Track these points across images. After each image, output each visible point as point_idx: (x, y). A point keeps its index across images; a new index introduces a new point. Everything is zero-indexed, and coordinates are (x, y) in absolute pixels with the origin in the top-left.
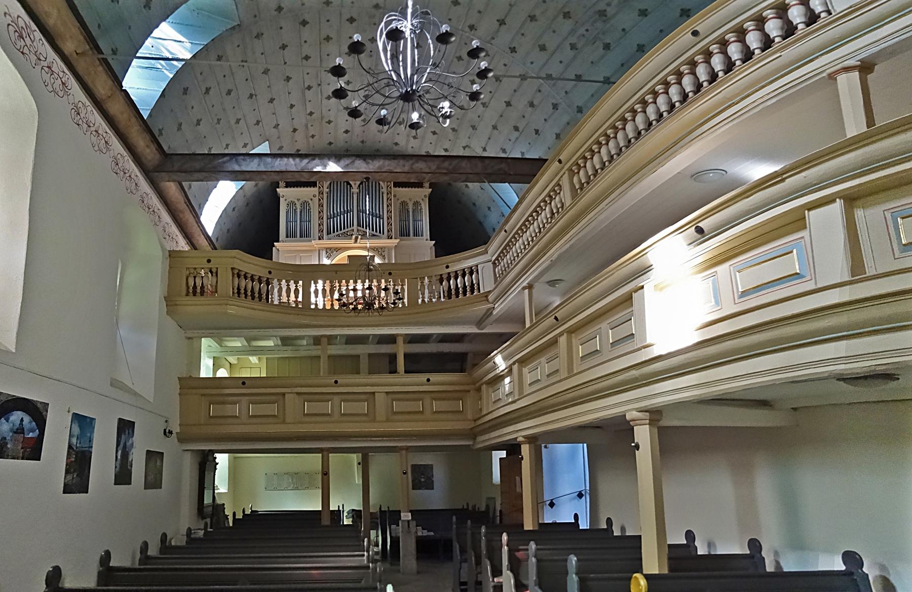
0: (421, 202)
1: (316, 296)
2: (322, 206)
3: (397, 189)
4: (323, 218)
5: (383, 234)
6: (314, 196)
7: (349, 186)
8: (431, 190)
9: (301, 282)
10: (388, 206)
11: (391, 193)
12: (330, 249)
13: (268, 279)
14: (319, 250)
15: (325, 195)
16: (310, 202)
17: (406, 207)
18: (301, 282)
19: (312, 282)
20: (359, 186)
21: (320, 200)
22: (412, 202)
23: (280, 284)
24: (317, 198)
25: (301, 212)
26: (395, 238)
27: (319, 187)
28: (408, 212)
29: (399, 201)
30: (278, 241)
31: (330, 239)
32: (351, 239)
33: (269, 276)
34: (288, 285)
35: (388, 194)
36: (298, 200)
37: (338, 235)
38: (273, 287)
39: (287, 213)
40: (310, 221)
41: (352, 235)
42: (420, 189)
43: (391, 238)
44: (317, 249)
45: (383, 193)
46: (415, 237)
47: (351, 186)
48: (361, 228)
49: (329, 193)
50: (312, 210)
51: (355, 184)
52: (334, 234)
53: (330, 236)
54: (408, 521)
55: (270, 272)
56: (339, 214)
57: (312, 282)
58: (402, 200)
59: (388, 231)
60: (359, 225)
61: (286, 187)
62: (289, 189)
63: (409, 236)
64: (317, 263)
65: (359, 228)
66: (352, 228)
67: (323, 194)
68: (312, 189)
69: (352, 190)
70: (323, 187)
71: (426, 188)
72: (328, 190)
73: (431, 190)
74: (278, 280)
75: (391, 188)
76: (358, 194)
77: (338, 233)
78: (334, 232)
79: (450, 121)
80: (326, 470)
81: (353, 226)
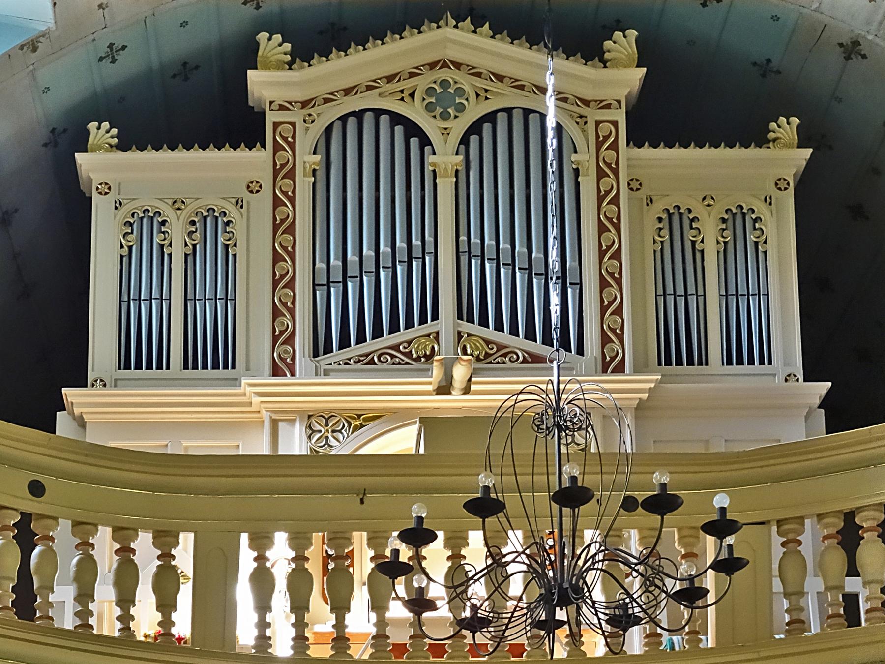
0: (762, 210)
1: (263, 606)
2: (291, 230)
3: (646, 152)
4: (291, 285)
5: (580, 351)
6: (253, 188)
7: (414, 142)
8: (808, 152)
9: (187, 540)
10: (602, 229)
11: (616, 173)
12: (327, 417)
13: (26, 518)
14: (274, 423)
15: (303, 185)
16: (233, 213)
17: (689, 235)
18: (187, 540)
19: (244, 538)
20: (464, 141)
21: (277, 203)
22: (718, 211)
23: (86, 545)
24: (266, 195)
25: (189, 258)
26: (637, 371)
27: (277, 148)
28: (699, 254)
29: (657, 209)
30: (81, 381)
31: (326, 373)
32: (426, 372)
33: (31, 505)
34: (125, 552)
35: (601, 174)
36: (177, 204)
37: (367, 360)
38: (50, 555)
39: (125, 260)
40: (230, 299)
41: (429, 358)
42: (753, 152)
43: (620, 369)
44: (266, 416)
45: (577, 172)
46: (735, 368)
47: (425, 141)
48: (475, 329)
49: (321, 175)
50: (240, 251)
51: (446, 132)
52: (347, 353)
53: (325, 360)
54: (843, 588)
55: (37, 489)
56: (369, 265)
57: (244, 538)
58: (669, 203)
59: (605, 340)
60: (463, 312)
61: (123, 146)
62: (134, 156)
63: (704, 360)
64: (266, 451)
65: (466, 327)
66: (430, 327)
67: (291, 175)
68: (242, 154)
69: (430, 159)
70: (292, 146)
71: (788, 146)
72: (318, 158)
73: (808, 152)
74: (76, 524)
75: (614, 146)
76: (461, 178)
77: (364, 348)
78: (344, 343)
79: (829, 613)
80: (408, 192)
81: (435, 317)
